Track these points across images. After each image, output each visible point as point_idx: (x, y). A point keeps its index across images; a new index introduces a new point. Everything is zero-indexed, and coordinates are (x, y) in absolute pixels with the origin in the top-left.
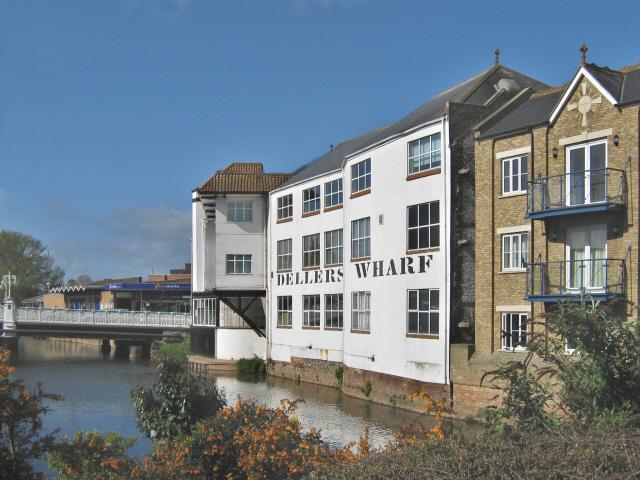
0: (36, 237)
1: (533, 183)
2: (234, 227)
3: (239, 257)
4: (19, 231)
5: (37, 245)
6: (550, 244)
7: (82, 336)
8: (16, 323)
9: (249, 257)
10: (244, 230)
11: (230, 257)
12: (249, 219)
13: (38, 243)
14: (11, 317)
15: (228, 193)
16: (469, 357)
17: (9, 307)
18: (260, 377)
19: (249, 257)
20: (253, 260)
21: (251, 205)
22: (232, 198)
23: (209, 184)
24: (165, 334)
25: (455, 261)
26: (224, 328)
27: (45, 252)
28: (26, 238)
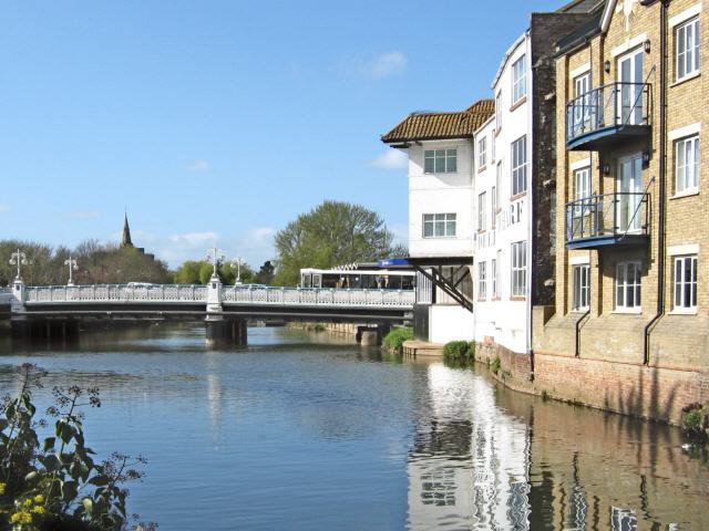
0: (369, 207)
1: (626, 83)
2: (433, 180)
3: (440, 216)
4: (346, 201)
5: (371, 219)
6: (605, 179)
7: (337, 321)
8: (222, 305)
9: (453, 216)
10: (448, 183)
11: (427, 217)
12: (453, 169)
13: (373, 215)
14: (216, 296)
15: (424, 139)
16: (545, 322)
17: (214, 286)
18: (467, 363)
19: (453, 216)
20: (458, 220)
21: (453, 152)
22: (429, 145)
23: (399, 129)
24: (406, 316)
25: (540, 206)
26: (440, 305)
27: (382, 226)
28: (355, 209)
